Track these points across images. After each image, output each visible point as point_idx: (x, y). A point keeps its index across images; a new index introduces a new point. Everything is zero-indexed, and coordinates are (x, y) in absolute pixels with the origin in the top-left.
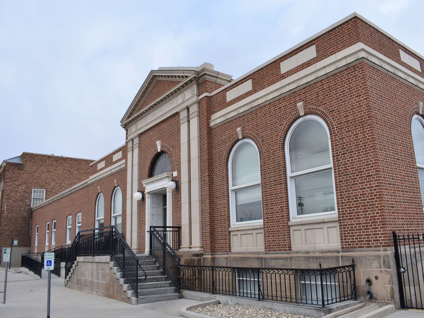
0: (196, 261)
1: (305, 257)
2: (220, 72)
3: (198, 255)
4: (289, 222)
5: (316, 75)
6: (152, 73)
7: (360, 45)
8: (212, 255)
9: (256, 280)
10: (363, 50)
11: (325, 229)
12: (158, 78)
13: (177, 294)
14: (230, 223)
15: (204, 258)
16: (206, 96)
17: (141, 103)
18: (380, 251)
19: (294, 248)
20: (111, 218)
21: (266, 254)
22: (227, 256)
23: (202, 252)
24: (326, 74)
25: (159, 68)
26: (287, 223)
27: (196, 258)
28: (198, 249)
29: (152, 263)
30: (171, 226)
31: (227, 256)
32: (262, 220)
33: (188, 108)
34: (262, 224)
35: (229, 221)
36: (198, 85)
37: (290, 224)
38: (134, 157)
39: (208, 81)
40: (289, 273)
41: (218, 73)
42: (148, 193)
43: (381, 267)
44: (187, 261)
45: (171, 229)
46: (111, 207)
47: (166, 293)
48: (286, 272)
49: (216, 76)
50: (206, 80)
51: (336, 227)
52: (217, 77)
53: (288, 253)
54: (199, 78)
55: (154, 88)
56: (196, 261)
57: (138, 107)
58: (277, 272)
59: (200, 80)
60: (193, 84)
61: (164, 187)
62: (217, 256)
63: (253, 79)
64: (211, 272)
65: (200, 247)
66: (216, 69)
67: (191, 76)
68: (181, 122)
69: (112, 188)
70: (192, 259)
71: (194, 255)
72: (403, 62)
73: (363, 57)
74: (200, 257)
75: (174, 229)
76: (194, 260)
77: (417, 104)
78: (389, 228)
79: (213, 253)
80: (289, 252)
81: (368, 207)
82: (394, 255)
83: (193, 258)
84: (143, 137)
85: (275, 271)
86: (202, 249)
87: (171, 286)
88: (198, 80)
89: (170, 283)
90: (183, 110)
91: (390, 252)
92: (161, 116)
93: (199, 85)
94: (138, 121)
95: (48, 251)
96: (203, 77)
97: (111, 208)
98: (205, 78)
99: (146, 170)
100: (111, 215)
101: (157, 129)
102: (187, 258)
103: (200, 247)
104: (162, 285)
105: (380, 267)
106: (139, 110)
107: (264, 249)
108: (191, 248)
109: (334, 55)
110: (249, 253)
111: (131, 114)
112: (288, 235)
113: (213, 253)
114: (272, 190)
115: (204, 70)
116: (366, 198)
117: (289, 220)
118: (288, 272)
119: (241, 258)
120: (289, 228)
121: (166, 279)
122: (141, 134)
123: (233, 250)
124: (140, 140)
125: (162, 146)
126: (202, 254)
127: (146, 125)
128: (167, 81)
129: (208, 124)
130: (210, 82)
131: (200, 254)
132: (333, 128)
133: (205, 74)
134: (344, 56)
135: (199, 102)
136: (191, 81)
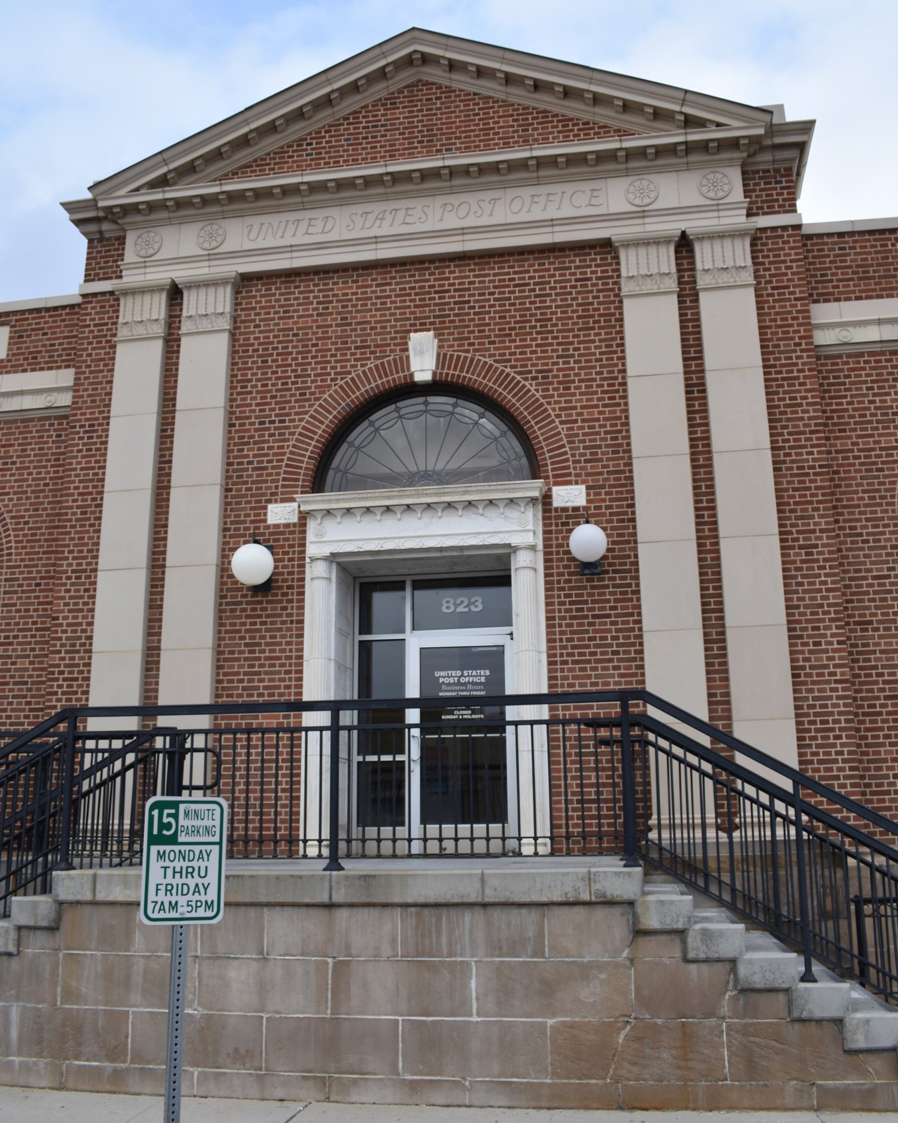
5: (49, 398)
17: (272, 143)
24: (881, 342)
30: (545, 691)
33: (175, 293)
45: (542, 711)
54: (763, 149)
55: (390, 102)
57: (244, 156)
60: (729, 163)
68: (123, 332)
75: (567, 710)
81: (834, 701)
92: (463, 231)
95: (204, 788)
101: (410, 280)
106: (225, 177)
109: (53, 373)
114: (29, 643)
128: (506, 104)
132: (6, 537)
134: (876, 317)
136: (733, 144)
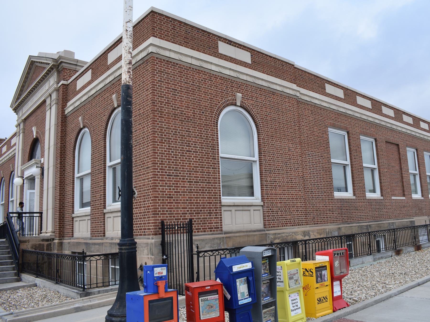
0: (45, 246)
1: (109, 243)
2: (79, 59)
3: (47, 240)
4: (104, 210)
6: (30, 59)
7: (152, 40)
8: (59, 240)
9: (82, 263)
10: (151, 45)
11: (233, 211)
12: (39, 65)
13: (16, 277)
14: (74, 209)
15: (54, 243)
16: (62, 84)
18: (149, 239)
19: (225, 228)
20: (9, 203)
21: (91, 239)
22: (69, 241)
23: (53, 237)
25: (40, 53)
26: (103, 210)
27: (46, 243)
28: (49, 234)
29: (5, 248)
31: (69, 241)
32: (90, 208)
34: (90, 211)
35: (73, 207)
36: (59, 72)
37: (105, 211)
38: (18, 142)
39: (67, 69)
40: (215, 254)
41: (77, 61)
42: (26, 178)
43: (148, 255)
44: (35, 247)
46: (9, 191)
47: (6, 277)
48: (223, 253)
49: (75, 63)
50: (64, 68)
51: (259, 210)
52: (76, 65)
53: (102, 239)
55: (34, 73)
56: (45, 246)
58: (223, 253)
59: (60, 68)
61: (32, 175)
62: (64, 241)
63: (92, 69)
64: (304, 246)
65: (52, 232)
66: (76, 57)
67: (51, 63)
69: (10, 173)
70: (40, 244)
71: (43, 240)
72: (222, 54)
73: (151, 52)
74: (50, 242)
76: (43, 245)
77: (234, 95)
78: (160, 218)
79: (61, 238)
80: (103, 238)
82: (160, 243)
83: (41, 242)
84: (28, 122)
85: (220, 251)
86: (54, 234)
87: (14, 270)
88: (58, 68)
89: (14, 267)
90: (47, 97)
91: (158, 239)
93: (59, 72)
94: (23, 106)
96: (61, 65)
97: (9, 192)
98: (62, 66)
99: (27, 155)
100: (9, 199)
102: (34, 243)
103: (52, 232)
104: (3, 269)
105: (148, 255)
107: (90, 235)
108: (47, 233)
110: (82, 238)
111: (18, 99)
112: (265, 216)
113: (61, 238)
115: (60, 57)
116: (161, 188)
117: (105, 208)
118: (213, 254)
119: (77, 243)
120: (104, 215)
121: (12, 263)
122: (26, 119)
123: (76, 235)
124: (24, 125)
125: (37, 133)
126: (53, 239)
127: (28, 110)
129: (63, 111)
130: (69, 69)
131: (51, 239)
133: (62, 62)
135: (57, 90)
